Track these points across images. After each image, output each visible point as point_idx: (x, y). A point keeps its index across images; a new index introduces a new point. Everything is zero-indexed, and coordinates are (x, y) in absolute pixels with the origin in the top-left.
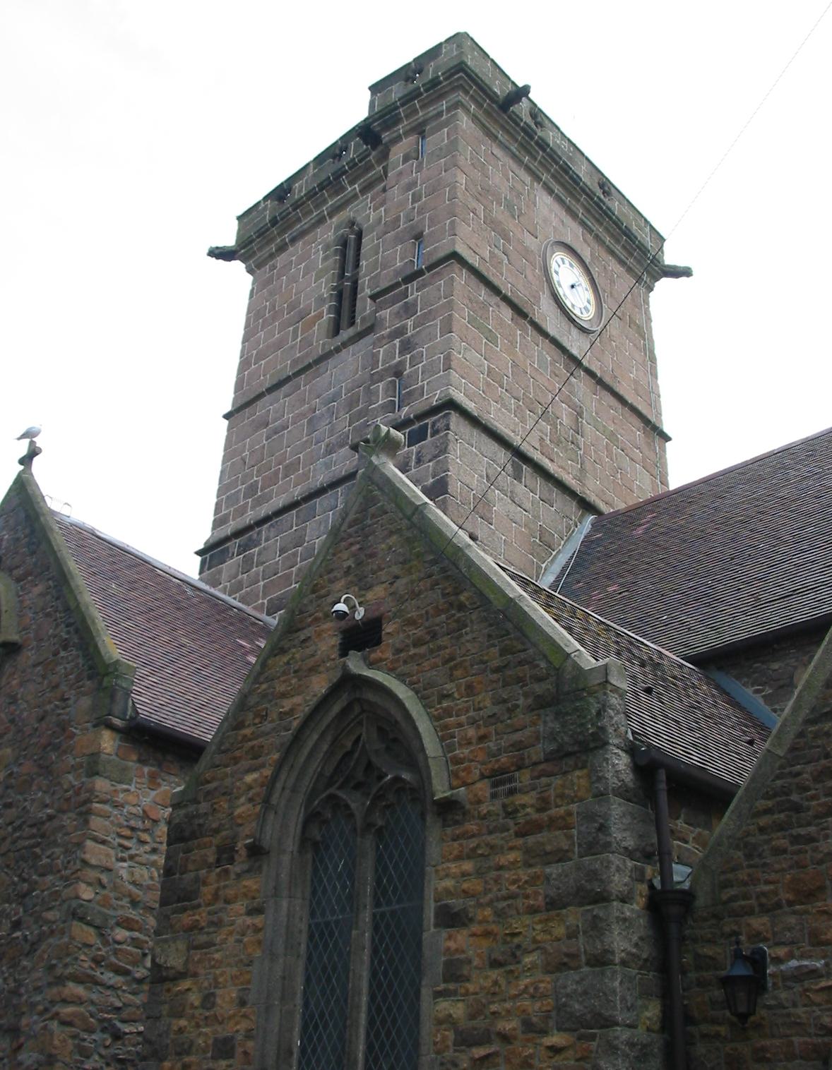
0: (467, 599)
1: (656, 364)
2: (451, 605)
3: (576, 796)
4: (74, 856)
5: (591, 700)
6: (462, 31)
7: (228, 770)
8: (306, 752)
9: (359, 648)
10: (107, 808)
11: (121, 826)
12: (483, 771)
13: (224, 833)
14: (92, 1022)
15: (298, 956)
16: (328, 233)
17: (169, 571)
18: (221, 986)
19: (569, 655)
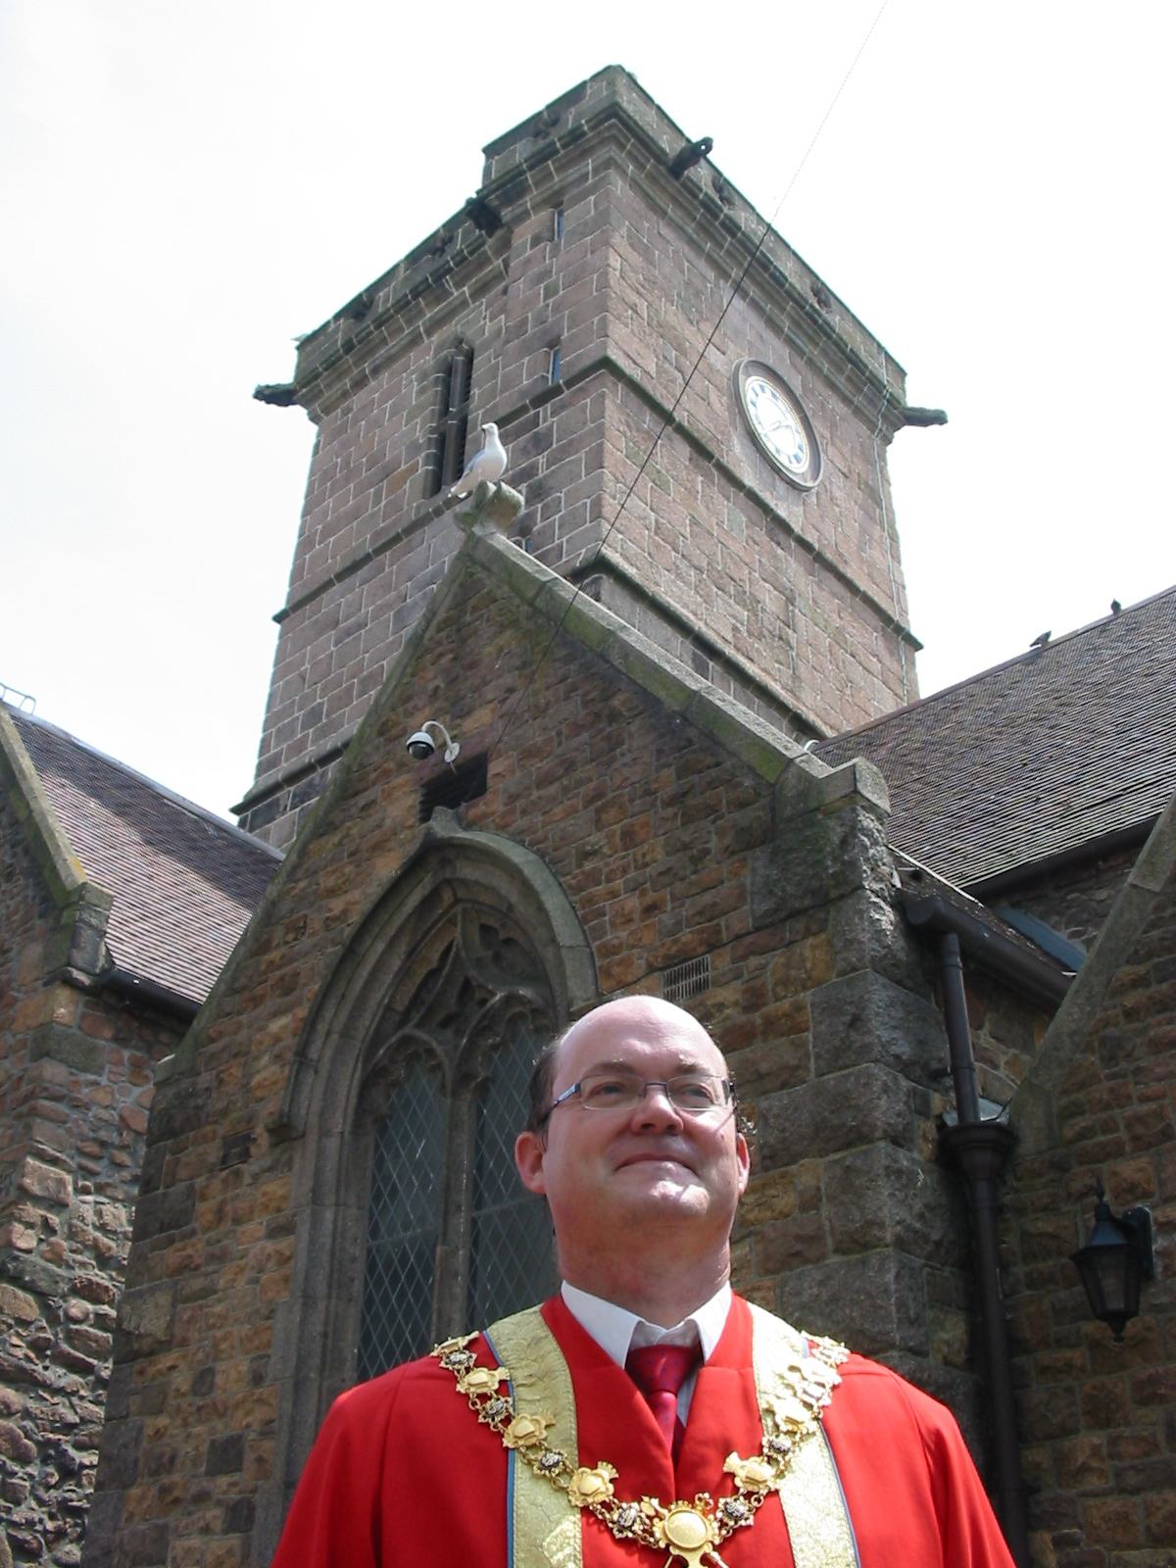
0: (623, 704)
1: (897, 542)
2: (597, 716)
3: (809, 978)
4: (7, 1182)
5: (831, 823)
6: (614, 62)
7: (244, 1018)
8: (365, 972)
9: (453, 804)
10: (62, 1108)
11: (85, 1139)
12: (651, 959)
13: (234, 1115)
14: (26, 1446)
15: (350, 1300)
16: (426, 357)
17: (182, 803)
18: (224, 1356)
19: (791, 761)
